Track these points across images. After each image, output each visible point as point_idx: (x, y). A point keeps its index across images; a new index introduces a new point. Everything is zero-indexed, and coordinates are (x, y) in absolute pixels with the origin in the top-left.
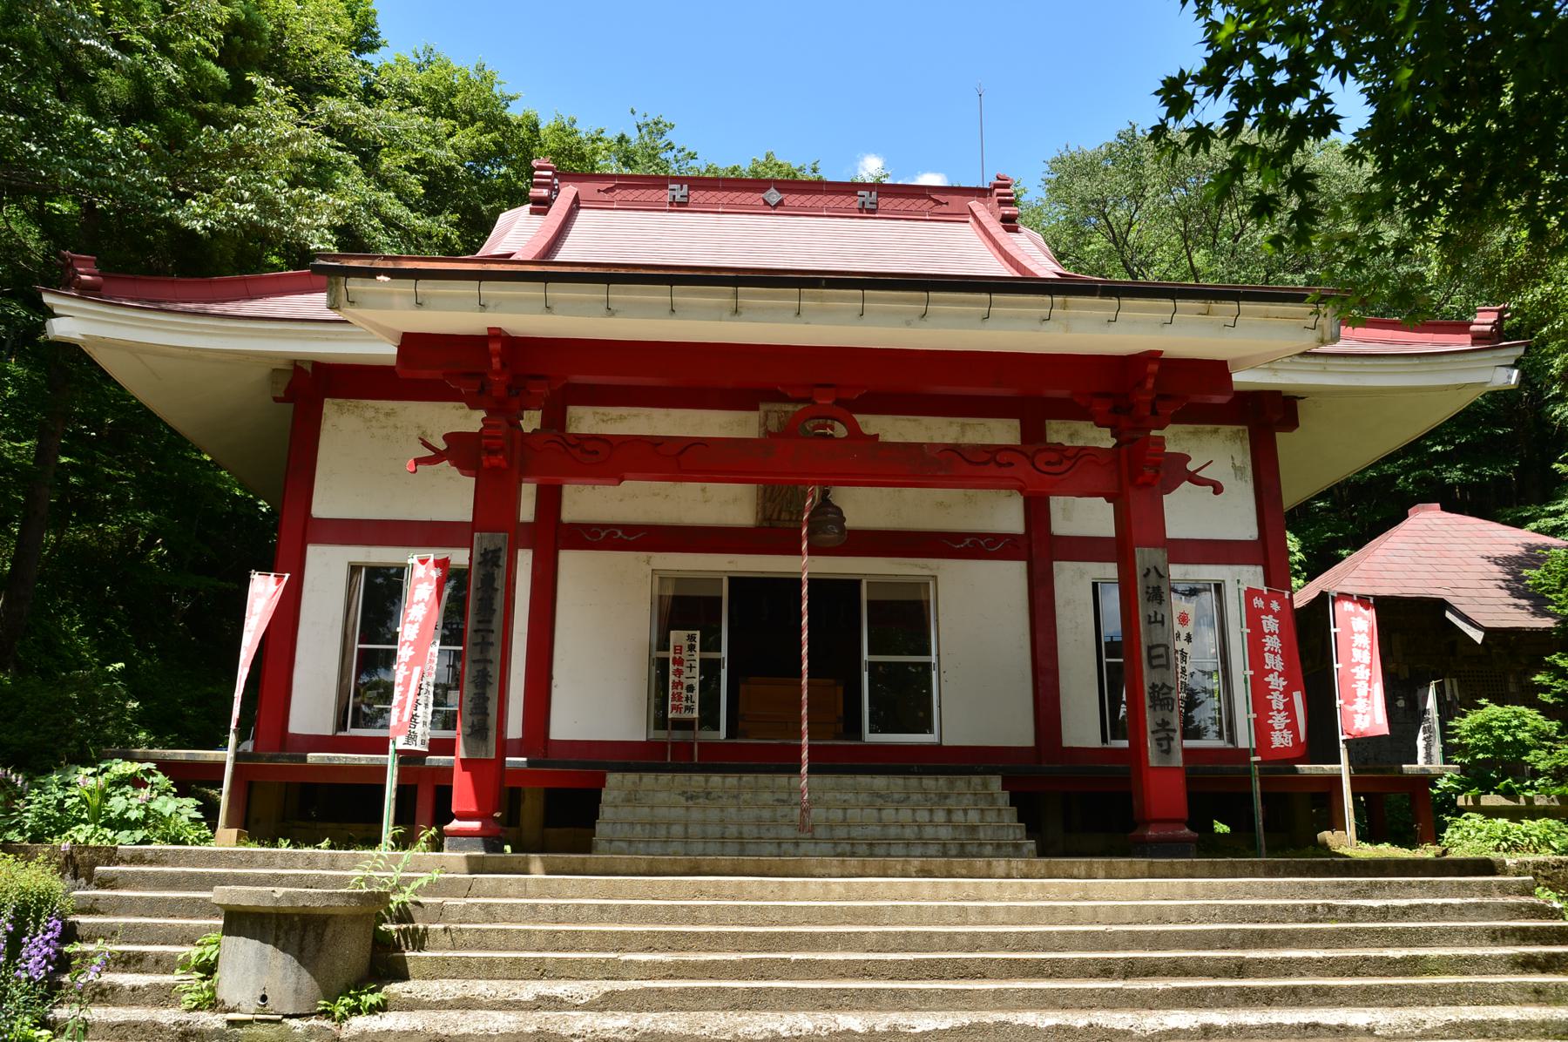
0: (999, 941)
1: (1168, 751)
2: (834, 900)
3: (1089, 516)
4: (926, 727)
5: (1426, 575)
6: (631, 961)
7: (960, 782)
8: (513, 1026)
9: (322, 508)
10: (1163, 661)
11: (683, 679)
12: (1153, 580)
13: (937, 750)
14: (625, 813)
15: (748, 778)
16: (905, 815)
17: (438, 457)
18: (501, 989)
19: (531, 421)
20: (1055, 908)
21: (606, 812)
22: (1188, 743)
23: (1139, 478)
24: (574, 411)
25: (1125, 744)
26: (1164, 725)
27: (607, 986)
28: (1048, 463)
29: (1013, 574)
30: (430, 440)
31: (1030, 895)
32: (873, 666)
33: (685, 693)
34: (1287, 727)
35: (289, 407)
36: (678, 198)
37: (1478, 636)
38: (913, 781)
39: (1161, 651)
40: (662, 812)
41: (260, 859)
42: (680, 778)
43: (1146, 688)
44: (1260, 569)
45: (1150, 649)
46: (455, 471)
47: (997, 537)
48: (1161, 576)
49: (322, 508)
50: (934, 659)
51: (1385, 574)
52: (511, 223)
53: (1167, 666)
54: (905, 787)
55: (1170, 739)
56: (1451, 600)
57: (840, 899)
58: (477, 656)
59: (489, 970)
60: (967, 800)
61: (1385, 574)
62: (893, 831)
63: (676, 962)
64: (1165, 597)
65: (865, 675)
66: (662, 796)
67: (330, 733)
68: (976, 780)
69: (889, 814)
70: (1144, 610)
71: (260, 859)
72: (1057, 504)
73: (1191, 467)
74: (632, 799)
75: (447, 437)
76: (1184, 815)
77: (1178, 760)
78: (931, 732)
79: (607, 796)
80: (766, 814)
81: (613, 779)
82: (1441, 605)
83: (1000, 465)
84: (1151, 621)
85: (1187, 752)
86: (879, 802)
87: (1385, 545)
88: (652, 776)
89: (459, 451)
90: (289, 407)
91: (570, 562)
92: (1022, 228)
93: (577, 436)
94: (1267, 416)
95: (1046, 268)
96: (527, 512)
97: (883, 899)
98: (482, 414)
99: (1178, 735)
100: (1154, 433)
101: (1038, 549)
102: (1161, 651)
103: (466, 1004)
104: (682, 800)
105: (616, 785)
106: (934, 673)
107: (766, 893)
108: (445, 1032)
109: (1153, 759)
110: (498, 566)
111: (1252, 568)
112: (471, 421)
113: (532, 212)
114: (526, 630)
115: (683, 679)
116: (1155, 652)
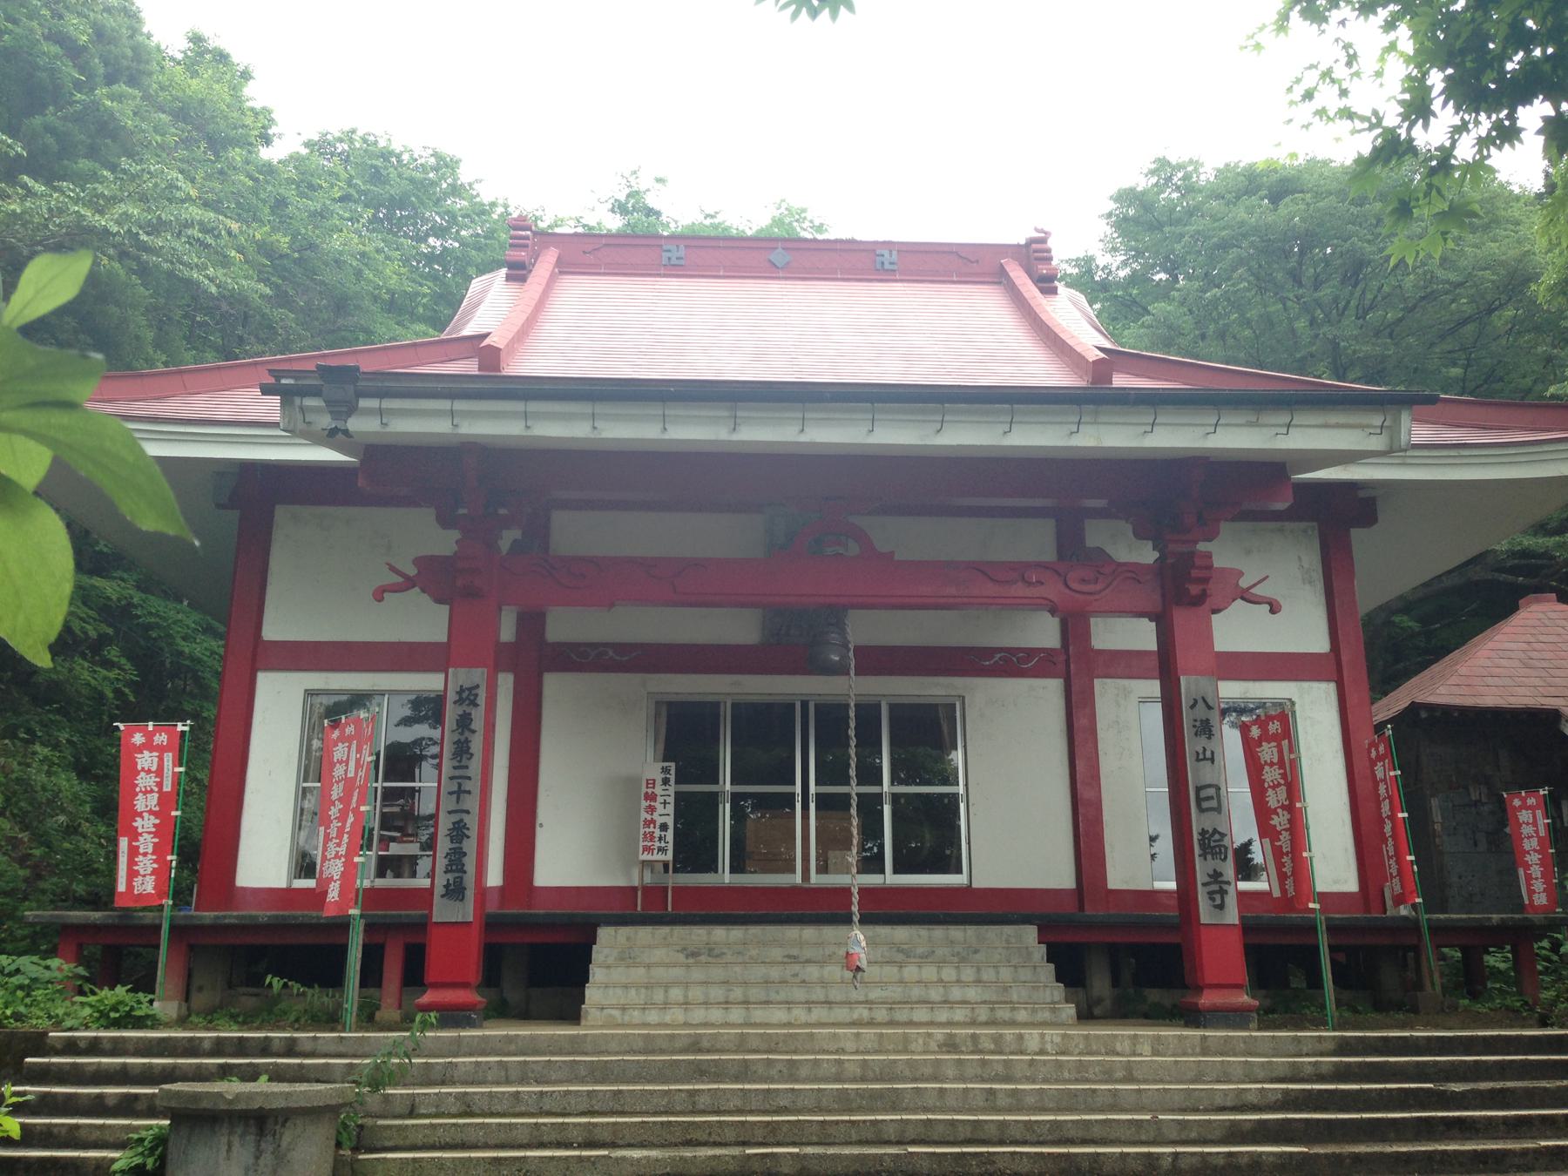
1: (1221, 907)
4: (950, 864)
5: (1537, 682)
6: (624, 1158)
7: (992, 933)
9: (273, 630)
10: (1214, 803)
12: (1201, 711)
13: (967, 891)
14: (618, 974)
15: (755, 931)
16: (929, 972)
17: (408, 584)
20: (1094, 1091)
21: (597, 973)
22: (1243, 886)
23: (1182, 592)
26: (1216, 876)
29: (1051, 689)
30: (399, 567)
31: (1066, 1075)
33: (657, 833)
35: (234, 515)
36: (674, 261)
39: (1212, 792)
40: (659, 973)
41: (207, 1045)
42: (679, 931)
43: (1196, 836)
45: (1198, 789)
47: (1031, 652)
49: (273, 630)
50: (961, 789)
51: (1490, 681)
52: (484, 291)
53: (1218, 809)
57: (854, 1080)
61: (1490, 681)
62: (916, 992)
66: (659, 954)
67: (283, 884)
70: (1191, 745)
73: (1244, 583)
74: (627, 958)
75: (417, 561)
77: (1232, 916)
78: (959, 871)
79: (599, 953)
80: (775, 973)
81: (605, 934)
83: (1030, 584)
85: (1243, 896)
86: (900, 957)
87: (1490, 645)
88: (649, 929)
90: (234, 515)
91: (555, 686)
94: (1336, 516)
96: (507, 633)
100: (1202, 547)
101: (1076, 668)
102: (1212, 792)
104: (681, 957)
105: (608, 942)
106: (962, 806)
107: (773, 1072)
109: (1206, 915)
111: (1323, 685)
113: (509, 278)
116: (1203, 794)
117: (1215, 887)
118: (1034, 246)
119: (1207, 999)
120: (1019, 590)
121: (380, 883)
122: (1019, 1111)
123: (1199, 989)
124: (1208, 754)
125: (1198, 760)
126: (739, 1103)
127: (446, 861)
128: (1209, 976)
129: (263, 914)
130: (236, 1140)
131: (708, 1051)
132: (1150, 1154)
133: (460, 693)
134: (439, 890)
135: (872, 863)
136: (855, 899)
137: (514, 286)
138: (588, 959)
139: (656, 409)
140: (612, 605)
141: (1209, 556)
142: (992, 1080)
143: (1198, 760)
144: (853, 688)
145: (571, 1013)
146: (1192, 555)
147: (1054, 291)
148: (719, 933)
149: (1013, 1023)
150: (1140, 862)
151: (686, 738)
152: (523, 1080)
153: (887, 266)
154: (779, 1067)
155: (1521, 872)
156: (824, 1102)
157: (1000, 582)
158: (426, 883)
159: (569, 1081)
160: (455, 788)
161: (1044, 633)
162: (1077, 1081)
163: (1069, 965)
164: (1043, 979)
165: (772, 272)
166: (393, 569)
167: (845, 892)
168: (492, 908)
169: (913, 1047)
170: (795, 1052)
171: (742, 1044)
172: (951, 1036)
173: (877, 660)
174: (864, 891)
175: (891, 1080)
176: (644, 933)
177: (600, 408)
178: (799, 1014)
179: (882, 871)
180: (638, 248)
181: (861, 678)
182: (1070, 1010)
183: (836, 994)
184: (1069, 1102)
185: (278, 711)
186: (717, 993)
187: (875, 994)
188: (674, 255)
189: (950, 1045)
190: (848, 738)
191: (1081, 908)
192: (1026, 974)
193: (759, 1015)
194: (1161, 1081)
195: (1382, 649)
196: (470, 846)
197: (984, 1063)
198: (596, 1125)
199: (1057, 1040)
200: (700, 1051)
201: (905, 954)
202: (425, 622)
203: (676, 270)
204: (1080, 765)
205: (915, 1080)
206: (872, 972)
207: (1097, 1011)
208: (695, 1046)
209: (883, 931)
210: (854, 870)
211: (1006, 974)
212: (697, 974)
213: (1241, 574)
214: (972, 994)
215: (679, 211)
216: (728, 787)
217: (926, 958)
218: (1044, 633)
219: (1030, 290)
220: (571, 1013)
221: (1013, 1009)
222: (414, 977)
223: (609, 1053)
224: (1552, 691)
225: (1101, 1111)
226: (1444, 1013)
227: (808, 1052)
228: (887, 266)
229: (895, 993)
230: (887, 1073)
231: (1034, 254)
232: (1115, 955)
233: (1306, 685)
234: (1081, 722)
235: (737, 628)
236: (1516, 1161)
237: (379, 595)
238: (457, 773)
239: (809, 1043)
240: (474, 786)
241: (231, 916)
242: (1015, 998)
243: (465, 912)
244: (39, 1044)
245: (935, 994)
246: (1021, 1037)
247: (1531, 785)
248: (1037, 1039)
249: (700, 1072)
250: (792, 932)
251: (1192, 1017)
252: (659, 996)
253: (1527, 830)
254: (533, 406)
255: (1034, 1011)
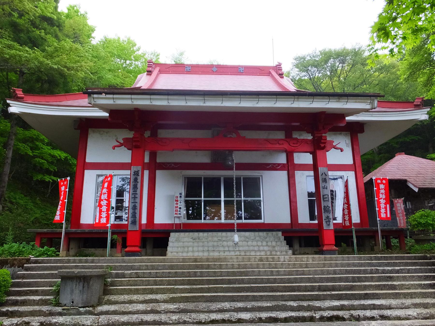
0: (282, 281)
1: (329, 225)
2: (235, 269)
3: (305, 158)
4: (260, 218)
5: (401, 173)
6: (178, 288)
7: (270, 233)
8: (144, 308)
9: (88, 160)
10: (327, 199)
11: (178, 206)
12: (324, 176)
13: (263, 224)
14: (176, 244)
15: (210, 233)
16: (255, 243)
17: (121, 145)
18: (141, 297)
19: (147, 134)
20: (298, 270)
21: (170, 244)
22: (334, 222)
23: (318, 147)
24: (160, 131)
25: (316, 222)
26: (328, 217)
27: (171, 295)
28: (294, 144)
29: (284, 174)
31: (291, 267)
32: (245, 201)
33: (179, 210)
34: (385, 213)
36: (188, 70)
37: (416, 190)
38: (257, 233)
40: (186, 244)
41: (72, 261)
44: (354, 172)
45: (323, 196)
46: (126, 149)
47: (279, 164)
48: (326, 175)
52: (141, 78)
54: (255, 235)
55: (329, 221)
56: (409, 180)
57: (237, 269)
58: (133, 201)
59: (137, 292)
60: (272, 239)
62: (251, 248)
63: (191, 288)
64: (327, 181)
65: (243, 203)
66: (186, 239)
68: (274, 233)
69: (250, 243)
70: (322, 185)
71: (72, 261)
72: (295, 155)
73: (334, 144)
74: (178, 240)
76: (334, 243)
77: (332, 227)
78: (261, 219)
79: (170, 239)
80: (215, 244)
81: (172, 234)
82: (406, 181)
83: (280, 144)
84: (324, 188)
86: (247, 239)
87: (389, 165)
88: (183, 233)
89: (128, 144)
90: (79, 131)
92: (285, 77)
93: (160, 138)
94: (355, 130)
95: (292, 88)
97: (249, 269)
98: (133, 132)
99: (332, 220)
100: (323, 135)
101: (290, 168)
102: (327, 196)
103: (131, 302)
104: (192, 240)
105: (173, 236)
106: (262, 203)
108: (125, 310)
109: (325, 227)
110: (138, 175)
111: (352, 172)
112: (130, 135)
113: (147, 74)
114: (147, 193)
115: (178, 206)
116: (325, 197)
117: (327, 220)
118: (278, 66)
119: (325, 248)
120: (278, 146)
121: (116, 223)
122: (279, 275)
123: (323, 245)
124: (326, 187)
125: (323, 188)
126: (207, 274)
127: (131, 215)
128: (326, 242)
129: (87, 230)
130: (77, 284)
131: (199, 262)
132: (312, 286)
133: (134, 172)
134: (130, 222)
135: (240, 218)
136: (236, 226)
137: (148, 76)
138: (168, 241)
139: (183, 97)
140: (173, 150)
141: (326, 137)
142: (272, 268)
143: (323, 188)
144: (234, 173)
145: (165, 255)
146: (322, 136)
147: (283, 77)
148: (201, 234)
149: (276, 255)
150: (304, 217)
151: (192, 187)
152: (152, 269)
153: (241, 71)
154: (217, 266)
155: (398, 218)
156: (229, 274)
157: (271, 146)
158: (126, 223)
159: (163, 269)
160: (133, 196)
161: (282, 159)
162: (293, 268)
163: (289, 242)
164: (283, 244)
165: (213, 73)
166: (118, 141)
167: (233, 224)
168: (143, 228)
169: (251, 261)
170: (221, 262)
171: (208, 260)
172: (261, 258)
173: (241, 166)
174: (237, 224)
175: (246, 269)
176: (182, 234)
177: (170, 97)
178: (222, 253)
179: (242, 219)
180: (178, 68)
181: (237, 171)
182: (290, 252)
183: (231, 249)
184: (290, 273)
185: (90, 180)
186: (201, 249)
187: (241, 249)
188: (188, 69)
189: (261, 260)
190: (234, 185)
191: (292, 227)
192: (279, 243)
193: (211, 254)
194: (315, 268)
195: (366, 163)
196: (138, 211)
197: (270, 264)
198: (170, 280)
199: (288, 258)
200: (197, 262)
201: (247, 239)
202: (125, 156)
203: (188, 72)
204: (291, 192)
205: (252, 268)
206: (240, 243)
207: (296, 253)
208: (196, 260)
209: (243, 233)
210: (235, 219)
211: (274, 243)
212: (196, 244)
213: (333, 142)
214: (266, 248)
215: (189, 60)
216: (203, 198)
217: (253, 240)
218: (282, 159)
219: (277, 77)
220: (165, 255)
221: (276, 252)
222: (124, 246)
223: (174, 263)
224: (405, 175)
225: (300, 275)
226: (382, 252)
227: (224, 262)
228: (241, 71)
229: (246, 248)
230: (245, 267)
231: (278, 68)
232: (300, 239)
233: (347, 172)
234: (291, 182)
235: (203, 158)
236: (406, 287)
237: (114, 148)
238: (134, 193)
239: (225, 259)
240: (138, 196)
241: (79, 230)
242: (276, 249)
243: (137, 228)
244: (28, 261)
245: (256, 248)
246: (279, 258)
247: (399, 197)
248: (283, 258)
249: (197, 267)
250: (220, 234)
251: (321, 252)
252: (186, 249)
253: (399, 208)
254: (152, 97)
255: (281, 252)
